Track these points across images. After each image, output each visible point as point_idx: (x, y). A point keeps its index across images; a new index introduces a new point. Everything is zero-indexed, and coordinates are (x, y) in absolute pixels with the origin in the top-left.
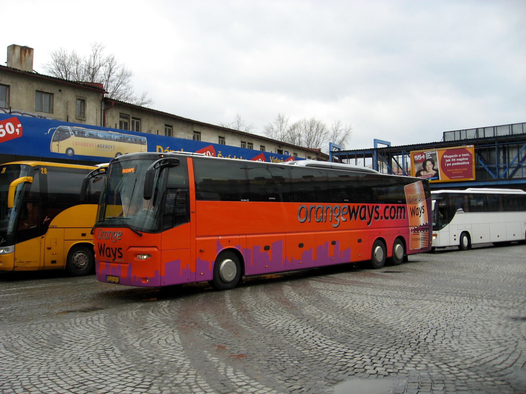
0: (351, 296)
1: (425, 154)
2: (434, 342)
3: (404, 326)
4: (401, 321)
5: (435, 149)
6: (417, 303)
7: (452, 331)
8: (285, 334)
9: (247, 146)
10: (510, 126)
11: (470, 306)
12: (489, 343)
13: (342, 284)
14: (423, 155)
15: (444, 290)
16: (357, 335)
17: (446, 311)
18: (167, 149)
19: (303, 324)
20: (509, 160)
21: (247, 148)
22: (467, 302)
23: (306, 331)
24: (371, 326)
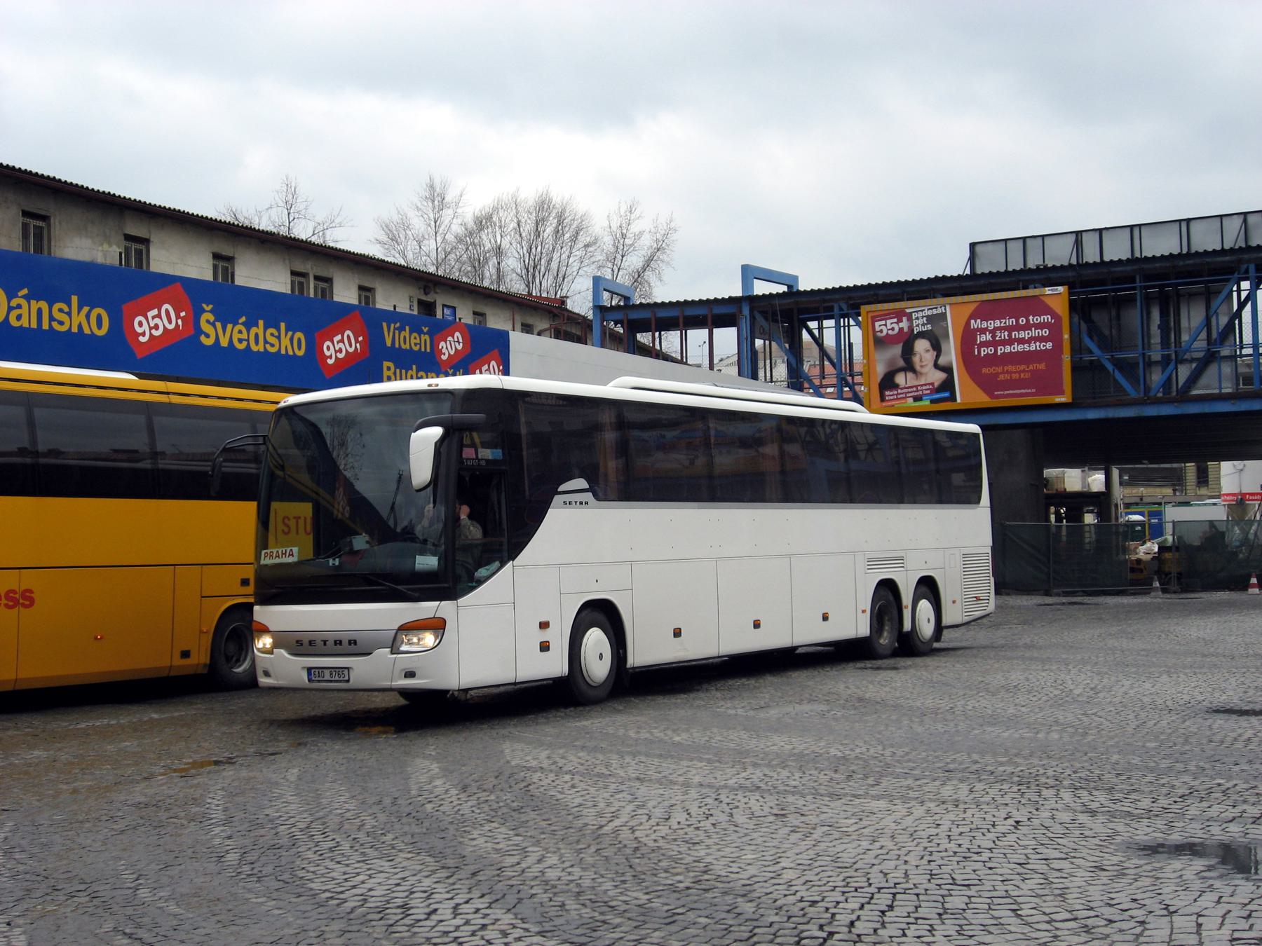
0: (634, 790)
1: (909, 316)
2: (880, 932)
3: (789, 884)
4: (784, 868)
5: (941, 300)
6: (845, 808)
7: (943, 896)
8: (391, 922)
9: (312, 286)
10: (1184, 225)
11: (1015, 812)
12: (1057, 929)
13: (611, 751)
14: (905, 319)
15: (941, 765)
16: (629, 919)
17: (936, 831)
18: (22, 297)
19: (455, 887)
20: (1180, 338)
21: (312, 295)
22: (1007, 799)
23: (465, 908)
24: (681, 885)
